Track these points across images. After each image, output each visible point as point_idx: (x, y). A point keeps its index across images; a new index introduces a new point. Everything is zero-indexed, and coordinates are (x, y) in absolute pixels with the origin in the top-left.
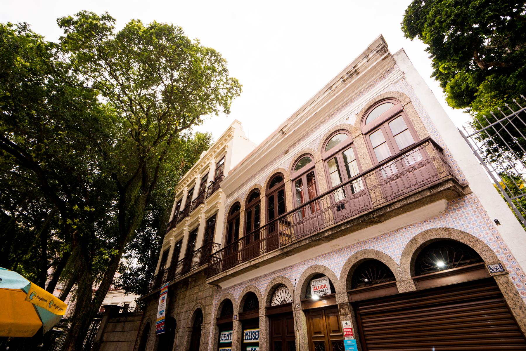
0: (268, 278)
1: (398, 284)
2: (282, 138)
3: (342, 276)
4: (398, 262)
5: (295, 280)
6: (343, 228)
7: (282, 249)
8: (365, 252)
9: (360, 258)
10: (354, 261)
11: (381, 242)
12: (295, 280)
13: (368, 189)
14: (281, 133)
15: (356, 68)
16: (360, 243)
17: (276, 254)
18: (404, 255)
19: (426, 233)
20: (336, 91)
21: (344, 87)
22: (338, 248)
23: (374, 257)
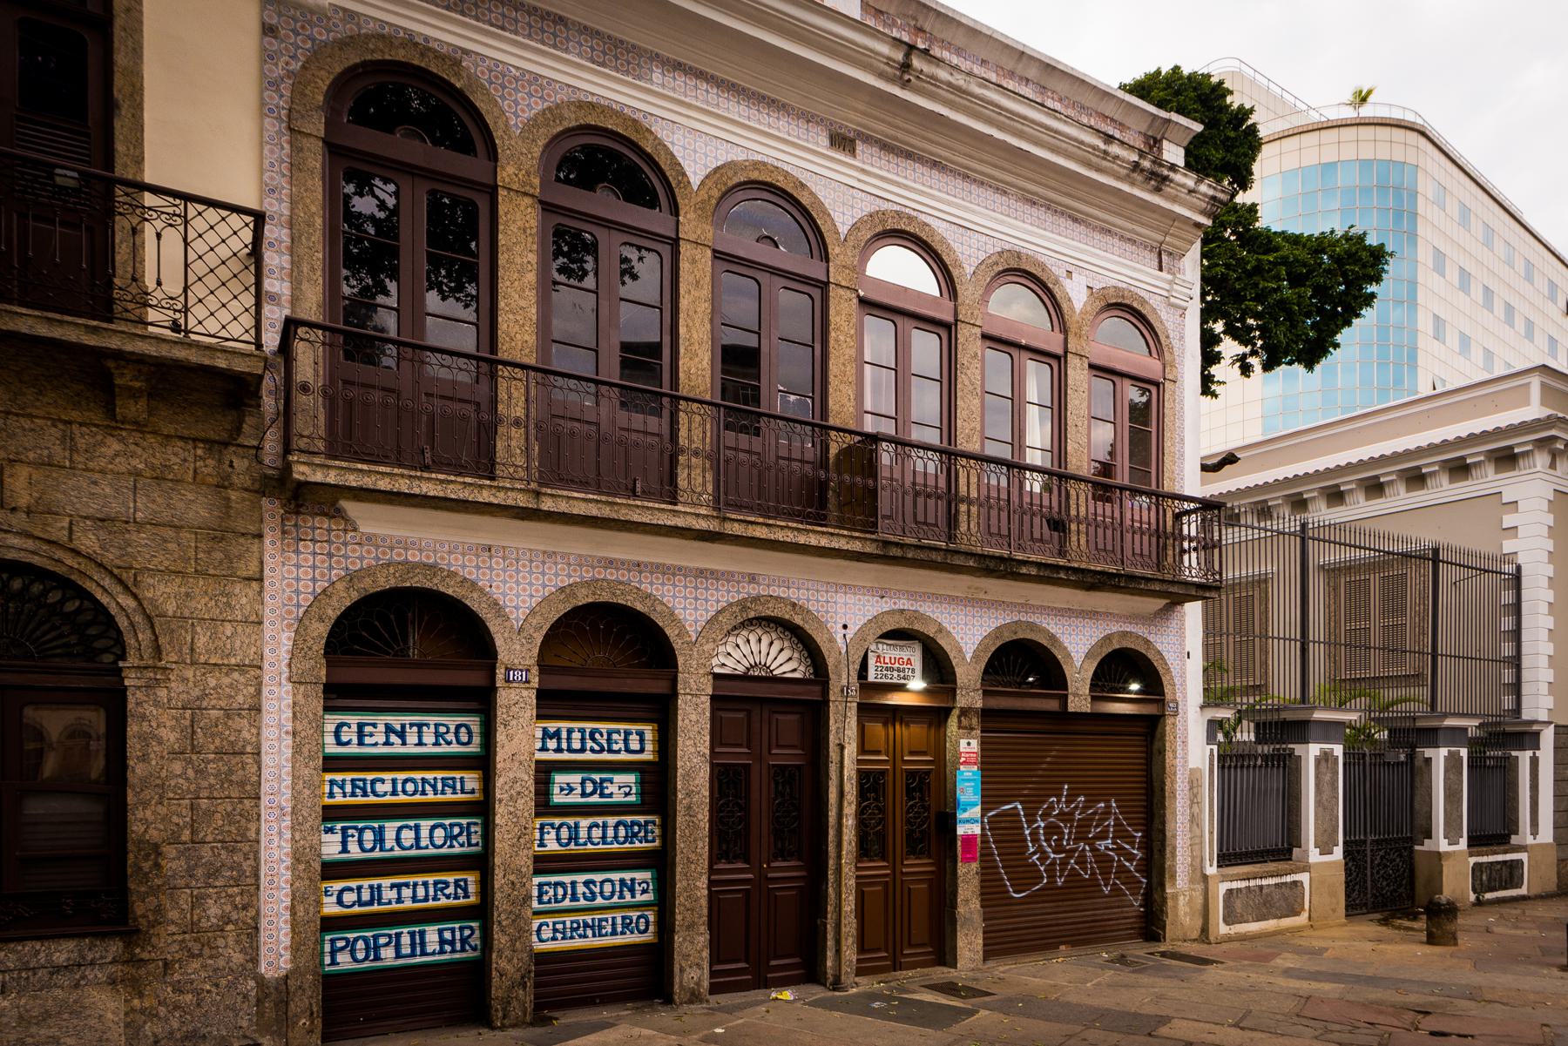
0: (723, 586)
1: (1070, 698)
2: (881, 75)
3: (975, 656)
4: (1078, 664)
5: (845, 627)
6: (1062, 575)
7: (886, 543)
8: (1032, 626)
9: (1021, 635)
10: (1008, 637)
11: (1063, 621)
12: (845, 627)
13: (956, 455)
14: (899, 56)
15: (1172, 175)
16: (1026, 607)
17: (856, 546)
18: (1088, 656)
19: (1125, 634)
20: (1105, 163)
21: (1118, 178)
22: (981, 596)
23: (1045, 642)
